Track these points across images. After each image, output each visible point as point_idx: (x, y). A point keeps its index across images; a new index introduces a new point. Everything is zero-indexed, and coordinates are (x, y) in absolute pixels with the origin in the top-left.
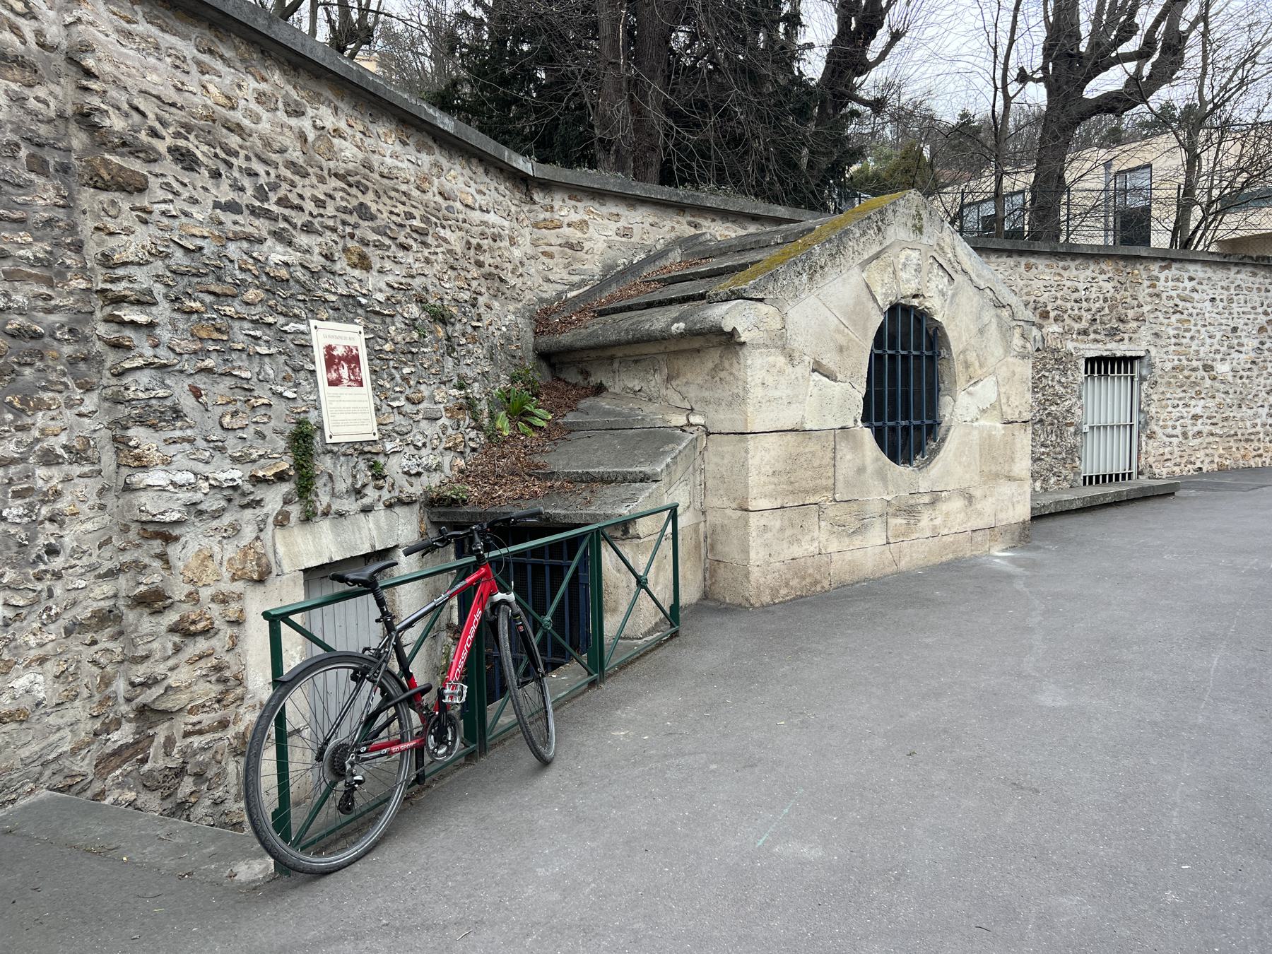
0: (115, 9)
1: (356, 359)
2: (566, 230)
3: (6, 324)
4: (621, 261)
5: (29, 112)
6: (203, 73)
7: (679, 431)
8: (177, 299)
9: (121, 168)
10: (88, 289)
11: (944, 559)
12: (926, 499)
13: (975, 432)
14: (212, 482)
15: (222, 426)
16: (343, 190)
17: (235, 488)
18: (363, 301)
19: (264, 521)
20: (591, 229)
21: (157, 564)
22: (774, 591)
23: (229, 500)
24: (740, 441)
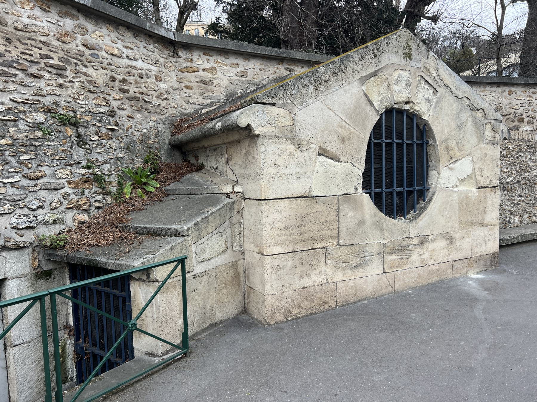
2: (201, 73)
11: (431, 281)
12: (416, 241)
13: (455, 195)
20: (219, 72)
22: (287, 312)
24: (259, 205)
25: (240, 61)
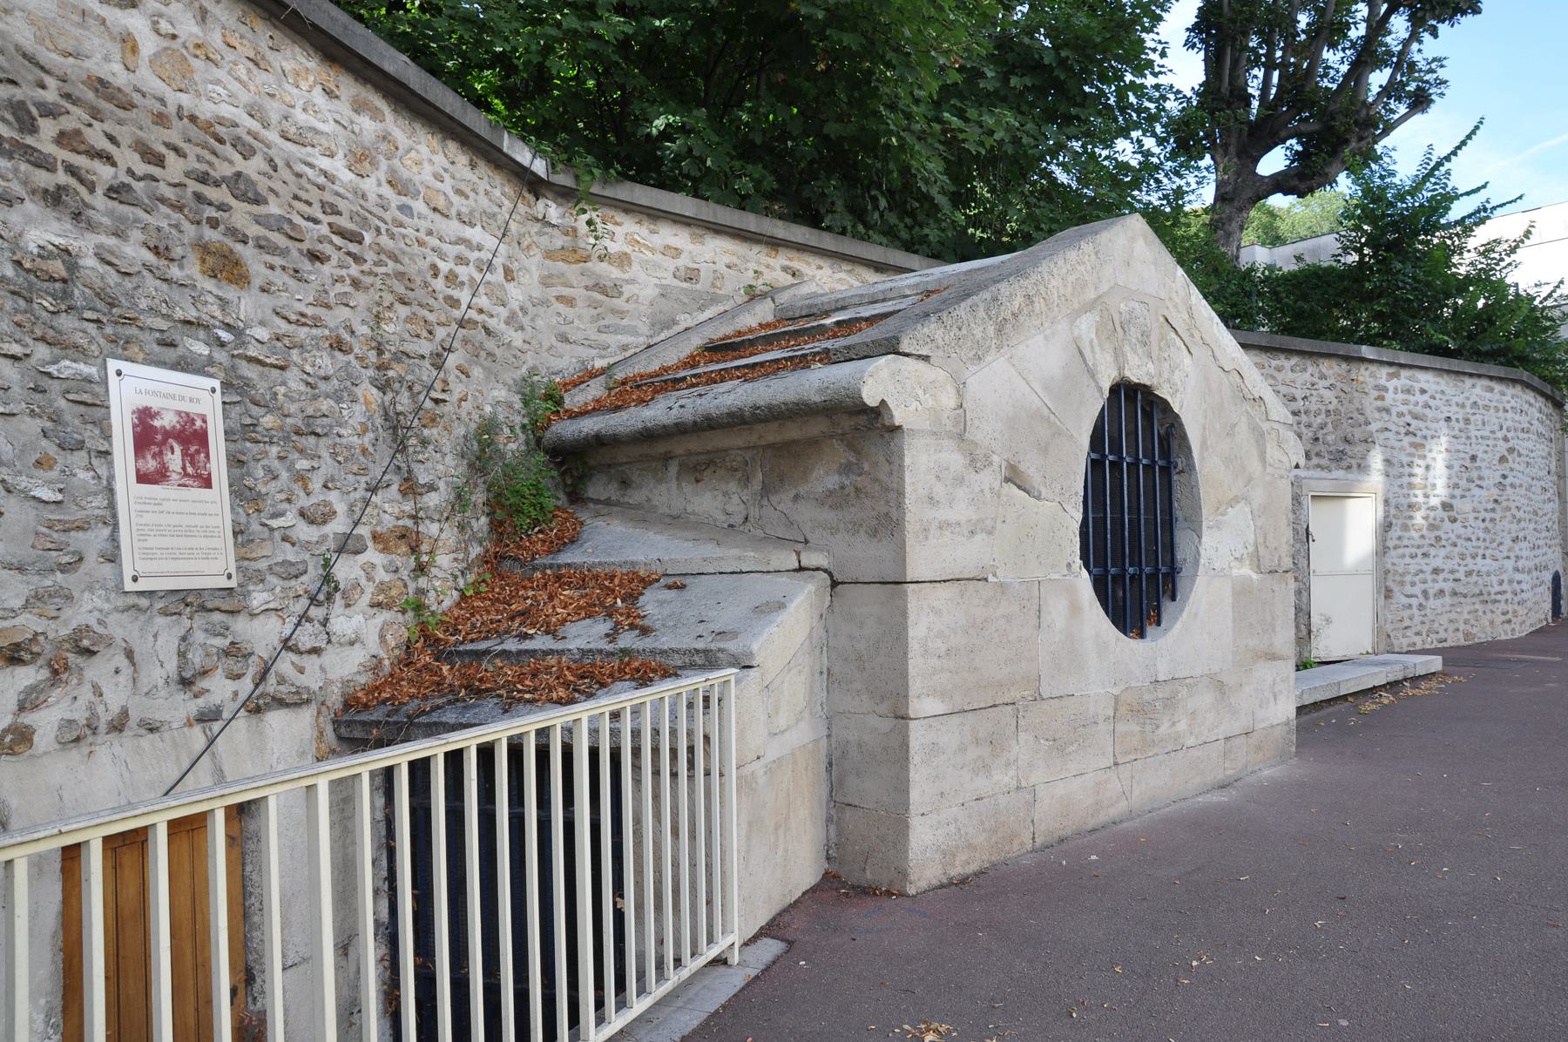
1: (201, 438)
20: (636, 266)
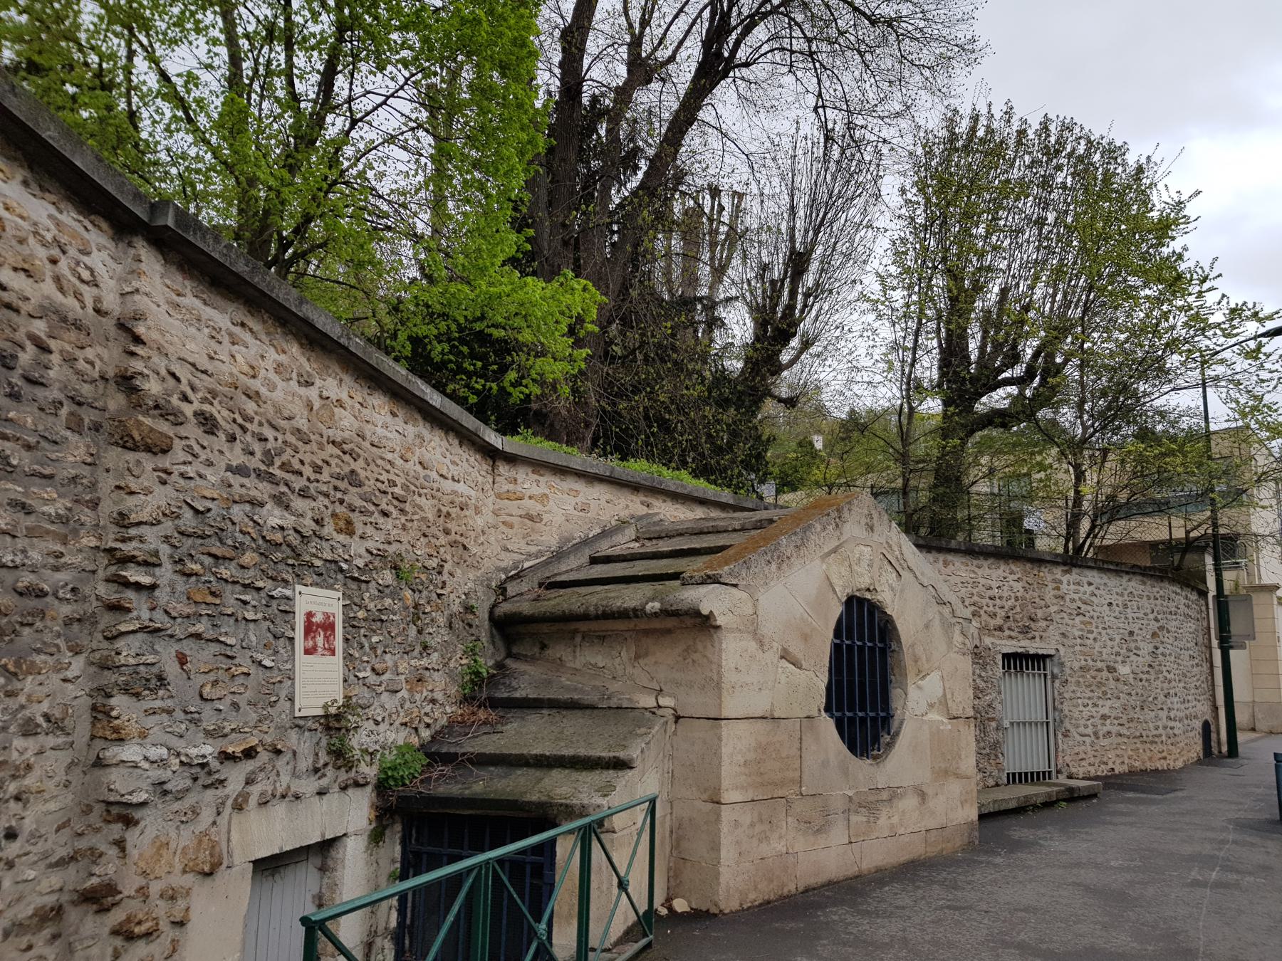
0: (169, 282)
2: (527, 503)
3: (17, 581)
4: (577, 534)
5: (77, 373)
6: (233, 343)
7: (648, 714)
8: (181, 560)
9: (152, 430)
10: (97, 548)
12: (885, 796)
14: (183, 759)
15: (201, 696)
16: (338, 457)
17: (203, 766)
18: (345, 566)
19: (223, 804)
20: (551, 502)
21: (113, 852)
23: (195, 779)
25: (580, 486)
